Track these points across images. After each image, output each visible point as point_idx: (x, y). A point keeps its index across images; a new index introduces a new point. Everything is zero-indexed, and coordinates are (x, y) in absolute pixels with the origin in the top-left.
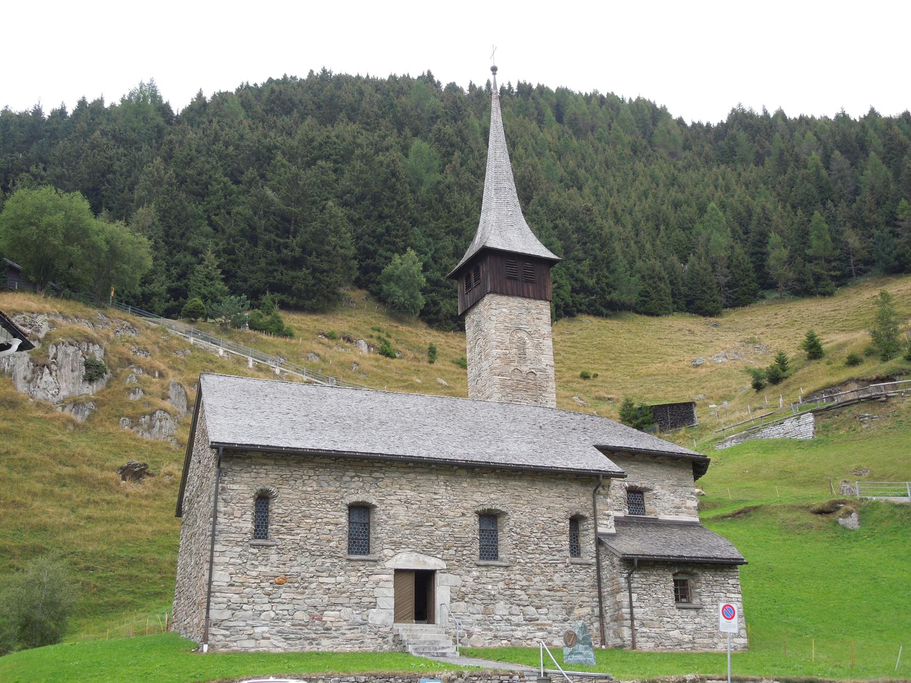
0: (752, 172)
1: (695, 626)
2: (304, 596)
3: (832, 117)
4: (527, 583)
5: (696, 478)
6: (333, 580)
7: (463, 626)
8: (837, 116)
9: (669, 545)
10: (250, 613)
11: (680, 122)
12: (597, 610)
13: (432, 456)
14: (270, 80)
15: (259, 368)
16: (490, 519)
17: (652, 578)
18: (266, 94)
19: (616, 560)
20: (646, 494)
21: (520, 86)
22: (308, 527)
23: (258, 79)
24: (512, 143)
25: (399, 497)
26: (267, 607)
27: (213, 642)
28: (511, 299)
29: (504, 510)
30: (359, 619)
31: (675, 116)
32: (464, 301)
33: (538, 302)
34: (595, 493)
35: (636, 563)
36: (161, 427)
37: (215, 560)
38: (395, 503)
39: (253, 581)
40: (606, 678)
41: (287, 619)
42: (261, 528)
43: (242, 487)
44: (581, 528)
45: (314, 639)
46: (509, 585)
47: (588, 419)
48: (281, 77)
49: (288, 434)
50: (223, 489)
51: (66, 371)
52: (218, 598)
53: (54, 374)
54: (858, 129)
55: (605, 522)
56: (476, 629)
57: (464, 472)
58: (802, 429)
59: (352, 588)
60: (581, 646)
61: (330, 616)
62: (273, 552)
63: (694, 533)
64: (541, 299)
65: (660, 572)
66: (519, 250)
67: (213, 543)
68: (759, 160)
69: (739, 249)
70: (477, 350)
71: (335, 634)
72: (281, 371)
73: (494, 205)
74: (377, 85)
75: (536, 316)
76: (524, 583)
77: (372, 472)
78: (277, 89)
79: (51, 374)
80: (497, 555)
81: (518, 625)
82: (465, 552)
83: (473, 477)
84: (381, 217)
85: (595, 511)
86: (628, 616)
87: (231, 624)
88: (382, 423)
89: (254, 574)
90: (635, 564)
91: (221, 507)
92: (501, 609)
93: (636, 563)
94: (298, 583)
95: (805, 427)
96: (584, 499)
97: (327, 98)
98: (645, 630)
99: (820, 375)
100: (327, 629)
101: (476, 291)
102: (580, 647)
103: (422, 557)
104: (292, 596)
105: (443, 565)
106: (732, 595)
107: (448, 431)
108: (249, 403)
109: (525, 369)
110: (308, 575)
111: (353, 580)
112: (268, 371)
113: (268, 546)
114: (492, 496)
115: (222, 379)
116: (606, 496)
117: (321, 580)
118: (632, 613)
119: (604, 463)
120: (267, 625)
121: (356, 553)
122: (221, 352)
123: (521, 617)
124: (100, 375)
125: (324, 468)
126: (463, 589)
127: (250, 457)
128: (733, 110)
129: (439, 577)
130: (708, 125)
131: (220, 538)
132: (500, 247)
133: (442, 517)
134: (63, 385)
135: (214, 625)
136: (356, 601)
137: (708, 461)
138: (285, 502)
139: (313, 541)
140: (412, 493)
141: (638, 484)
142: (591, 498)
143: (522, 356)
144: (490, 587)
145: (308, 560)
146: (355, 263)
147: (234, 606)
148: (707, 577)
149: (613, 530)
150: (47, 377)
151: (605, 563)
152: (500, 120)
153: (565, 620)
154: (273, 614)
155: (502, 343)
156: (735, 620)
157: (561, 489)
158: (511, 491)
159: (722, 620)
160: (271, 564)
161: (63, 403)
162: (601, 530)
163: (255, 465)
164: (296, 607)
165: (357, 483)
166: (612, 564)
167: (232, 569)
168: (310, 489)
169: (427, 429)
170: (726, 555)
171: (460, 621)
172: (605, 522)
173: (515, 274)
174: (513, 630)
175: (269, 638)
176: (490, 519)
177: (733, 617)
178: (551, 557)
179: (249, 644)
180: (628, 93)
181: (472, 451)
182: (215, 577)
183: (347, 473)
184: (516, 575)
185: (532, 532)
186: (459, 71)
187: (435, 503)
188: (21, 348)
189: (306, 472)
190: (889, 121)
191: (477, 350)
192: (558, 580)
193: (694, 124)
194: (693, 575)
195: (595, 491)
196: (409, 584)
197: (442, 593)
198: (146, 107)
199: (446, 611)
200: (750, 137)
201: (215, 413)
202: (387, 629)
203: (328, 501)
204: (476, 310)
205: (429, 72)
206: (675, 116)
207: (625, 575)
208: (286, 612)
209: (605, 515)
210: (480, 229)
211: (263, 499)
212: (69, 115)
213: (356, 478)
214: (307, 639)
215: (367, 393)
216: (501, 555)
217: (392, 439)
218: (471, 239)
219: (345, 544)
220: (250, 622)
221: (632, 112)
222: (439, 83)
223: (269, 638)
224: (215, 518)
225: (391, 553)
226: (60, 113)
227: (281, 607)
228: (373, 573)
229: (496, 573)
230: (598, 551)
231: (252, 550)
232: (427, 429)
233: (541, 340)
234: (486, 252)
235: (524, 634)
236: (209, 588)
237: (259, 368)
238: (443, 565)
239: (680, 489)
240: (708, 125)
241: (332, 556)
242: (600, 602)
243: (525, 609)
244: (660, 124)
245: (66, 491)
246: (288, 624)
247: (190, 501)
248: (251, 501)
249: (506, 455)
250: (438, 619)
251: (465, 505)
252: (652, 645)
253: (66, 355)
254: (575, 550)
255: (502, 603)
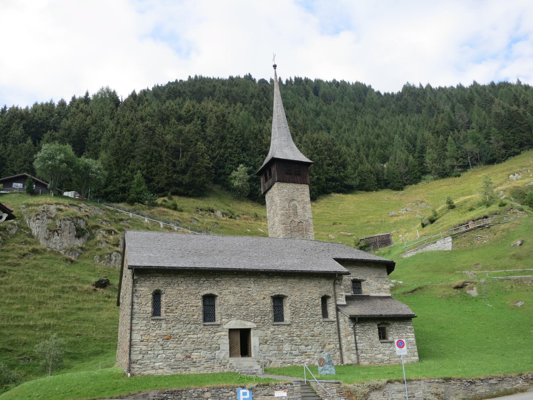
0: (416, 118)
1: (390, 352)
2: (181, 345)
3: (455, 86)
4: (300, 333)
5: (389, 273)
6: (195, 336)
7: (267, 358)
8: (458, 86)
9: (375, 309)
10: (152, 355)
11: (378, 93)
12: (338, 346)
13: (246, 268)
14: (169, 83)
15: (166, 228)
16: (278, 301)
17: (366, 327)
18: (166, 90)
19: (347, 319)
20: (362, 283)
21: (296, 78)
22: (182, 308)
23: (163, 82)
24: (287, 107)
25: (229, 291)
26: (161, 352)
27: (133, 372)
28: (289, 184)
29: (286, 295)
30: (210, 356)
31: (376, 90)
32: (264, 187)
33: (303, 185)
34: (334, 284)
35: (357, 320)
36: (116, 260)
37: (133, 328)
38: (227, 294)
39: (153, 338)
40: (338, 383)
41: (172, 358)
42: (156, 311)
43: (146, 290)
44: (328, 302)
45: (187, 368)
46: (290, 334)
47: (330, 245)
48: (174, 81)
49: (170, 260)
50: (136, 290)
51: (66, 233)
52: (136, 348)
53: (60, 235)
54: (469, 91)
55: (340, 299)
56: (274, 359)
57: (264, 276)
58: (446, 245)
59: (206, 340)
60: (327, 366)
61: (195, 355)
62: (164, 322)
63: (388, 302)
64: (304, 184)
65: (370, 324)
66: (291, 159)
67: (132, 319)
68: (419, 111)
69: (411, 158)
70: (272, 212)
71: (198, 365)
72: (178, 229)
73: (277, 136)
74: (222, 82)
75: (302, 192)
76: (298, 333)
77: (215, 278)
78: (172, 87)
79: (58, 235)
80: (283, 319)
81: (296, 356)
82: (266, 318)
83: (268, 278)
84: (226, 147)
85: (335, 293)
86: (354, 348)
87: (143, 362)
88: (220, 252)
89: (154, 334)
90: (357, 320)
91: (136, 301)
92: (287, 347)
93: (357, 320)
94: (179, 339)
95: (447, 244)
96: (328, 287)
97: (199, 89)
98: (364, 355)
99: (453, 219)
100: (194, 362)
101: (270, 181)
102: (327, 366)
103: (243, 322)
104: (175, 345)
105: (255, 325)
106: (410, 334)
107: (256, 254)
108: (146, 246)
109: (297, 220)
110: (183, 334)
111: (207, 335)
112: (170, 229)
113: (161, 320)
114: (279, 288)
115: (136, 232)
116: (340, 285)
117: (189, 336)
118: (356, 346)
119: (340, 268)
120: (162, 362)
121: (208, 321)
122: (146, 220)
123: (297, 351)
124: (84, 234)
125: (189, 277)
126: (266, 338)
127: (150, 273)
128: (404, 86)
129: (252, 332)
130: (392, 93)
131: (135, 316)
132: (281, 158)
133: (253, 300)
134: (64, 241)
135: (134, 363)
136: (208, 347)
137: (395, 263)
138: (169, 296)
139: (184, 316)
140: (237, 288)
141: (358, 278)
142: (332, 286)
143: (296, 214)
144: (280, 336)
145: (182, 326)
146: (213, 171)
147: (144, 352)
148: (396, 325)
149: (345, 303)
150: (57, 237)
151: (341, 320)
152: (279, 92)
153: (321, 352)
154: (164, 356)
155: (284, 207)
156: (405, 348)
157: (316, 282)
158: (289, 285)
159: (397, 349)
160: (164, 329)
161: (66, 250)
162: (339, 303)
163: (153, 277)
164: (177, 351)
165: (207, 284)
166: (345, 321)
167: (142, 333)
168: (182, 288)
169: (245, 254)
170: (406, 313)
171: (264, 355)
172: (340, 299)
173: (289, 171)
174: (293, 359)
175: (163, 369)
176: (278, 301)
177: (403, 346)
178: (312, 319)
179: (153, 372)
180: (351, 80)
181: (267, 264)
182: (133, 337)
183: (202, 279)
184: (293, 329)
185: (301, 306)
186: (261, 73)
187: (249, 292)
188: (7, 219)
189: (180, 279)
190: (484, 87)
191: (272, 212)
192: (317, 330)
193: (385, 94)
194: (388, 324)
195: (334, 283)
196: (237, 338)
197: (254, 341)
198: (109, 98)
199: (257, 349)
200: (415, 100)
201: (132, 251)
202: (226, 361)
203: (192, 294)
204: (270, 191)
205: (249, 74)
206: (376, 90)
207: (352, 326)
208: (171, 354)
209: (340, 295)
210: (271, 149)
211: (157, 295)
212: (67, 104)
213: (206, 282)
214: (183, 368)
215: (213, 236)
216: (286, 319)
217: (225, 260)
218: (266, 153)
219: (201, 317)
220: (153, 360)
221: (354, 89)
222: (255, 79)
223: (163, 369)
224: (132, 306)
225: (227, 320)
226: (62, 104)
227: (169, 352)
228: (217, 332)
229: (283, 329)
230: (337, 314)
231: (152, 322)
232: (245, 254)
233: (305, 205)
234: (274, 160)
235: (299, 360)
236: (130, 343)
237: (166, 228)
238: (255, 325)
239: (380, 280)
240: (392, 93)
241: (195, 324)
242: (340, 341)
243: (299, 347)
244: (368, 96)
245: (66, 295)
246: (173, 360)
247: (123, 297)
248: (151, 296)
249: (286, 266)
250: (253, 354)
251: (265, 293)
252: (368, 363)
253: (66, 225)
254: (325, 314)
255: (287, 344)
